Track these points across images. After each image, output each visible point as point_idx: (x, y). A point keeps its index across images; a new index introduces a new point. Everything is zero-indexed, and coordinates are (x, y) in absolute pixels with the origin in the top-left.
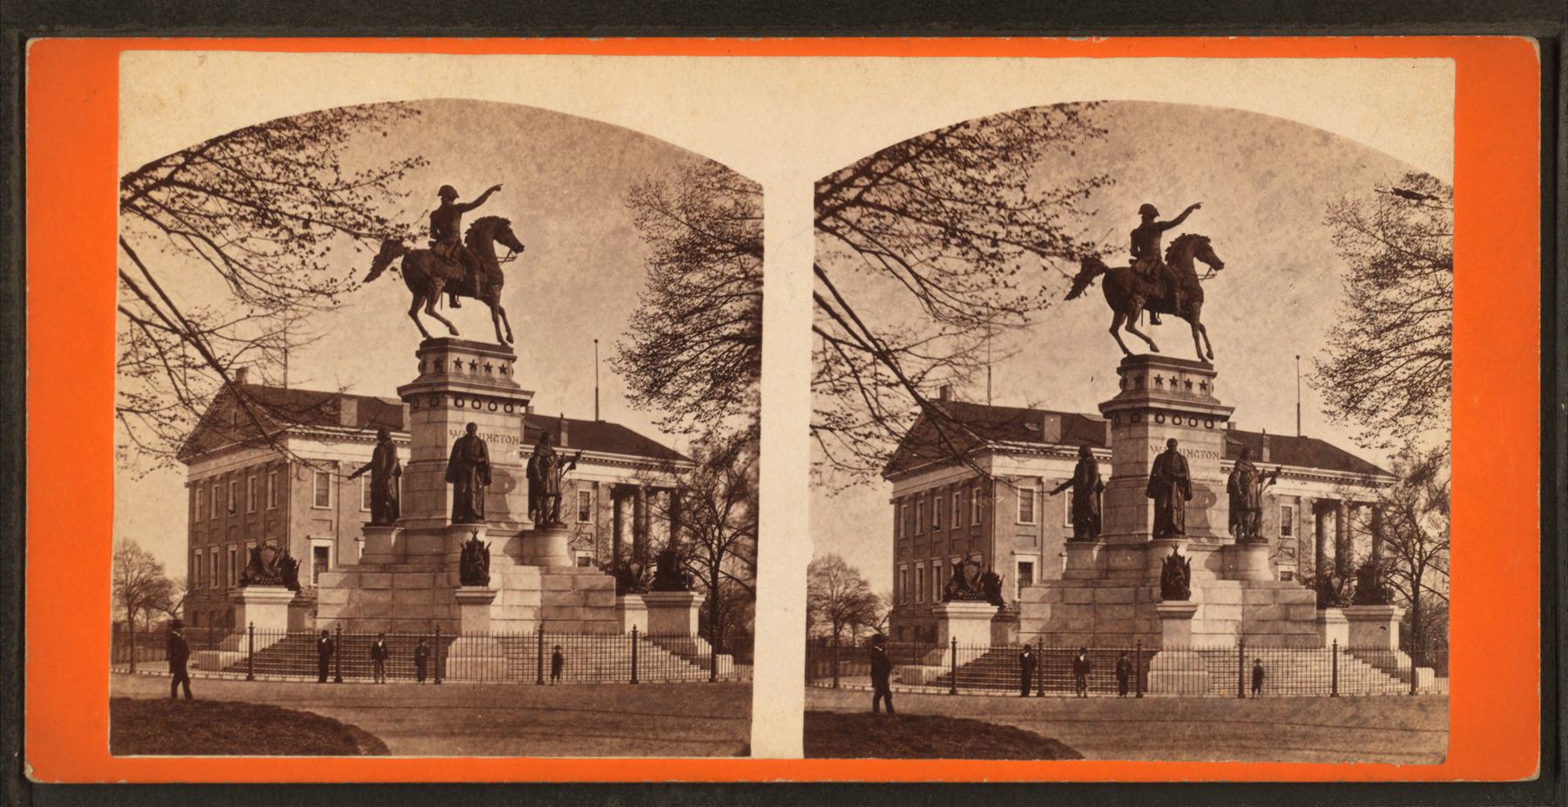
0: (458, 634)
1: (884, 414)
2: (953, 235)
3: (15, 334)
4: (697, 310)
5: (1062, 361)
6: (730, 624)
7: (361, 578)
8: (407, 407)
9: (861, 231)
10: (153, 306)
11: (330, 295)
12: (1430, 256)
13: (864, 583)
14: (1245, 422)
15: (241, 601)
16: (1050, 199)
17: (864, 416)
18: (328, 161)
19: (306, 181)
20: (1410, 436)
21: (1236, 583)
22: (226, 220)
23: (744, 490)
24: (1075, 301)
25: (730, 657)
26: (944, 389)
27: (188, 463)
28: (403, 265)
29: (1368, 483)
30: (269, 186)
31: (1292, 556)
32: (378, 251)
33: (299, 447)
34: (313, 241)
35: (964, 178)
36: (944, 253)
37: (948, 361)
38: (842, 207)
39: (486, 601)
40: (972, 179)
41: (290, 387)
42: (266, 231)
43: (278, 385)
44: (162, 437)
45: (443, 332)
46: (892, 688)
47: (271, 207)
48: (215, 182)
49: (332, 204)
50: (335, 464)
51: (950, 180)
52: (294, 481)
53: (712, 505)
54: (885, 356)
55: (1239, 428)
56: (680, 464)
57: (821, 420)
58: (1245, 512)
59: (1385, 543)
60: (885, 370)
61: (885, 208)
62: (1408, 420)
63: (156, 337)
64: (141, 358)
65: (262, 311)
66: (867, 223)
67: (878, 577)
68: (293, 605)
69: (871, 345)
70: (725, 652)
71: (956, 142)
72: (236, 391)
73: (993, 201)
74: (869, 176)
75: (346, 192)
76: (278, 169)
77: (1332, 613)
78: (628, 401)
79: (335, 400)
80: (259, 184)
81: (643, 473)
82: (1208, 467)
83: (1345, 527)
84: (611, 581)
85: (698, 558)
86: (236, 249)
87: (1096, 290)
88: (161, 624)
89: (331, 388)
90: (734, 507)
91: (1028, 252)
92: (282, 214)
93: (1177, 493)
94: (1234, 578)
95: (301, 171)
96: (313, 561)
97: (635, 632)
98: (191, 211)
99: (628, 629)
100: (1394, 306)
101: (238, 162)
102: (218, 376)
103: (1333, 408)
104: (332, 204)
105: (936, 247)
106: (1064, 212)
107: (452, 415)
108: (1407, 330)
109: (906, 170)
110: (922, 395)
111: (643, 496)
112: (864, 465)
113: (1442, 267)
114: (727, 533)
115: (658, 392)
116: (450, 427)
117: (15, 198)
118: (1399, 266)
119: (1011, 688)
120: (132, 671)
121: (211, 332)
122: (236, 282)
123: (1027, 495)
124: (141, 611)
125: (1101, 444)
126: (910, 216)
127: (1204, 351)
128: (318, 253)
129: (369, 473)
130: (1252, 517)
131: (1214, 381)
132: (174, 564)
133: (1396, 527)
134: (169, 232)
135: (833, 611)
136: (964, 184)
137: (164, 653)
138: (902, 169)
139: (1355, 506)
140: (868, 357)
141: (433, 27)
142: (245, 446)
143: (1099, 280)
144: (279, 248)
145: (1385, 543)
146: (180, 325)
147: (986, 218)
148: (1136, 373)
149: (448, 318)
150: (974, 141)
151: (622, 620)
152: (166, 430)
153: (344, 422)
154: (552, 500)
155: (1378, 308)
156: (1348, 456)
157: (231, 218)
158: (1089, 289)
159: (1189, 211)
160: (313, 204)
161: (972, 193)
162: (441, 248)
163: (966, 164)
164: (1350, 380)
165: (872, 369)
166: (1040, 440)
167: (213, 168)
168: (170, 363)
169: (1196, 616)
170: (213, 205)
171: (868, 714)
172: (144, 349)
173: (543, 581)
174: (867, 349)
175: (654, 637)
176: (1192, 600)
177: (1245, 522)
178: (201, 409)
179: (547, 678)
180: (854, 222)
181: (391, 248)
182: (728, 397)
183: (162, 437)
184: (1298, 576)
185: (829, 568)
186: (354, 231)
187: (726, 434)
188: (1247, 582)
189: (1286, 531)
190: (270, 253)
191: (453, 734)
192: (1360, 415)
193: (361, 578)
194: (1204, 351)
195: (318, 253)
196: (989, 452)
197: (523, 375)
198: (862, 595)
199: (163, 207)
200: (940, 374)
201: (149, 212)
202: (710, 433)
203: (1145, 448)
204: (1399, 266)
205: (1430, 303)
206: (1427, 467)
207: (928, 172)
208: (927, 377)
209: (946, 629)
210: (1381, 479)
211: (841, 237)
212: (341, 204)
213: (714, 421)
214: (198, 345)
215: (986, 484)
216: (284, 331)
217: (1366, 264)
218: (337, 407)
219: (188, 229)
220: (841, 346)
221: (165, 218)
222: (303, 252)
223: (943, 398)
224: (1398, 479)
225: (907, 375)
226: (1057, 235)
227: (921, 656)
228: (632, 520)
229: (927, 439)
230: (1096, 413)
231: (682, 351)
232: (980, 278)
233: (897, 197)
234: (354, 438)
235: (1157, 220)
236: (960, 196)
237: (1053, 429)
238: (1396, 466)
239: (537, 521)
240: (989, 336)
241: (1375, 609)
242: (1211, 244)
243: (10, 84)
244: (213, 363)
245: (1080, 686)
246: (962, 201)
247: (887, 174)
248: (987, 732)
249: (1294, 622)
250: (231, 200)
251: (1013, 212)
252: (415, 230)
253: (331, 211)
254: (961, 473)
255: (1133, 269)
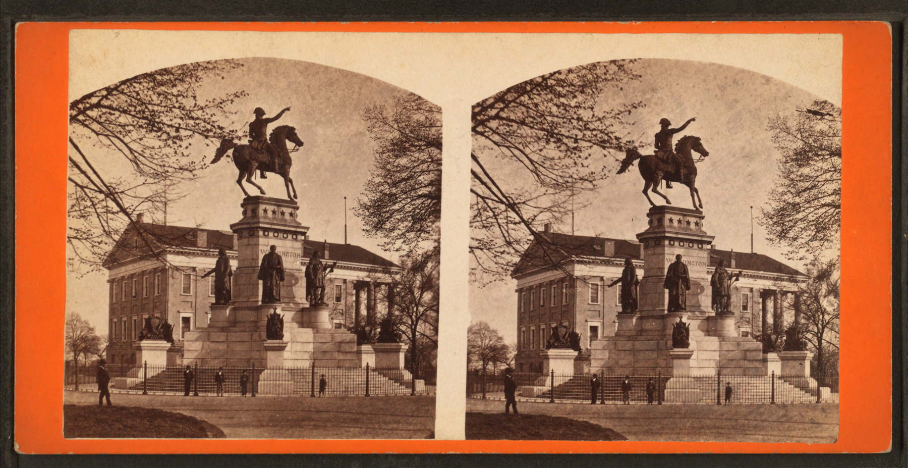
0: (265, 368)
1: (512, 240)
2: (552, 137)
3: (9, 194)
4: (403, 180)
5: (615, 209)
6: (423, 362)
7: (209, 335)
8: (236, 236)
9: (499, 134)
10: (89, 178)
11: (191, 171)
12: (828, 148)
13: (501, 338)
14: (721, 245)
15: (140, 349)
16: (608, 116)
17: (500, 241)
18: (190, 94)
19: (177, 105)
20: (817, 253)
21: (716, 338)
22: (131, 128)
23: (431, 284)
24: (623, 174)
25: (422, 381)
26: (546, 226)
27: (109, 269)
28: (233, 154)
29: (792, 280)
30: (156, 108)
31: (748, 322)
32: (219, 146)
33: (173, 259)
34: (181, 140)
35: (558, 103)
36: (547, 147)
37: (549, 209)
38: (488, 120)
39: (281, 348)
40: (563, 104)
41: (168, 224)
42: (154, 134)
43: (161, 223)
44: (94, 253)
45: (257, 193)
46: (517, 399)
47: (157, 120)
48: (125, 106)
49: (192, 118)
50: (194, 269)
51: (550, 104)
52: (170, 279)
53: (412, 293)
54: (512, 206)
55: (717, 248)
56: (394, 269)
57: (475, 244)
58: (721, 297)
59: (802, 315)
60: (512, 214)
61: (512, 121)
62: (816, 244)
63: (91, 196)
64: (82, 208)
65: (152, 181)
66: (502, 129)
67: (509, 334)
68: (170, 351)
69: (504, 200)
70: (420, 378)
71: (554, 83)
72: (136, 227)
73: (575, 117)
74: (503, 102)
75: (201, 111)
76: (161, 98)
77: (772, 356)
78: (364, 233)
79: (194, 232)
80: (150, 107)
81: (373, 274)
82: (699, 271)
83: (779, 306)
84: (354, 337)
85: (404, 323)
86: (137, 145)
87: (634, 168)
88: (93, 362)
89: (192, 225)
90: (425, 294)
91: (595, 146)
92: (163, 124)
93: (681, 286)
94: (714, 335)
95: (174, 99)
96: (181, 325)
97: (368, 367)
98: (111, 123)
99: (364, 365)
100: (807, 178)
101: (138, 94)
102: (126, 218)
103: (772, 236)
104: (192, 118)
105: (542, 143)
106: (616, 122)
107: (262, 241)
108: (815, 191)
109: (525, 99)
110: (534, 229)
111: (372, 288)
112: (500, 270)
113: (835, 155)
114: (421, 309)
115: (381, 227)
116: (260, 248)
117: (9, 115)
118: (810, 155)
119: (586, 399)
120: (77, 389)
121: (122, 192)
122: (137, 164)
123: (595, 287)
124: (82, 354)
125: (638, 258)
126: (527, 125)
127: (697, 204)
128: (184, 146)
129: (213, 274)
130: (725, 300)
131: (703, 221)
132: (101, 328)
133: (809, 306)
134: (98, 134)
135: (482, 354)
136: (558, 107)
137: (95, 379)
138: (522, 98)
139: (785, 293)
140: (503, 207)
141: (251, 16)
142: (142, 258)
143: (636, 162)
144: (162, 144)
145: (802, 315)
146: (104, 189)
147: (571, 126)
148: (658, 216)
149: (259, 184)
150: (564, 82)
151: (360, 360)
152: (96, 250)
153: (199, 245)
154: (320, 290)
155: (798, 178)
156: (780, 264)
157: (134, 126)
158: (630, 167)
159: (688, 122)
160: (181, 118)
161: (563, 112)
162: (255, 144)
163: (559, 95)
164: (782, 221)
165: (505, 214)
166: (603, 255)
167: (123, 97)
168: (98, 211)
169: (693, 357)
170: (124, 119)
171: (502, 414)
172: (83, 202)
173: (315, 337)
174: (502, 202)
175: (379, 370)
176: (690, 348)
177: (721, 303)
178: (117, 237)
179: (316, 393)
180: (494, 128)
181: (226, 144)
182: (422, 230)
183: (94, 253)
184: (752, 334)
185: (480, 330)
186: (205, 134)
187: (420, 252)
188: (722, 338)
189: (745, 308)
190: (156, 147)
191: (262, 426)
192: (787, 241)
193: (209, 335)
194: (697, 204)
195: (184, 146)
196: (573, 262)
197: (303, 217)
198: (499, 345)
199: (94, 120)
200: (545, 217)
201: (87, 123)
202: (411, 251)
203: (663, 260)
204: (810, 155)
205: (828, 176)
206: (826, 271)
207: (537, 100)
208: (537, 218)
209: (548, 365)
210: (799, 278)
211: (487, 137)
212: (197, 119)
213: (413, 244)
214: (115, 200)
215: (571, 281)
216: (165, 192)
217: (791, 153)
218: (195, 236)
219: (109, 133)
220: (487, 201)
221: (96, 126)
222: (176, 146)
223: (546, 231)
224: (809, 278)
225: (525, 217)
226: (612, 136)
227: (533, 380)
228: (366, 302)
229: (537, 255)
230: (635, 239)
231: (395, 203)
232: (568, 161)
233: (520, 115)
234: (205, 254)
235: (670, 128)
236: (556, 114)
237: (610, 249)
238: (808, 270)
239: (311, 302)
240: (573, 195)
241: (796, 353)
242: (701, 142)
243: (6, 49)
244: (123, 210)
245: (626, 398)
246: (557, 116)
247: (514, 101)
248: (572, 425)
249: (750, 361)
250: (134, 116)
251: (587, 123)
252: (240, 134)
253: (192, 122)
254: (557, 274)
255: (656, 156)
